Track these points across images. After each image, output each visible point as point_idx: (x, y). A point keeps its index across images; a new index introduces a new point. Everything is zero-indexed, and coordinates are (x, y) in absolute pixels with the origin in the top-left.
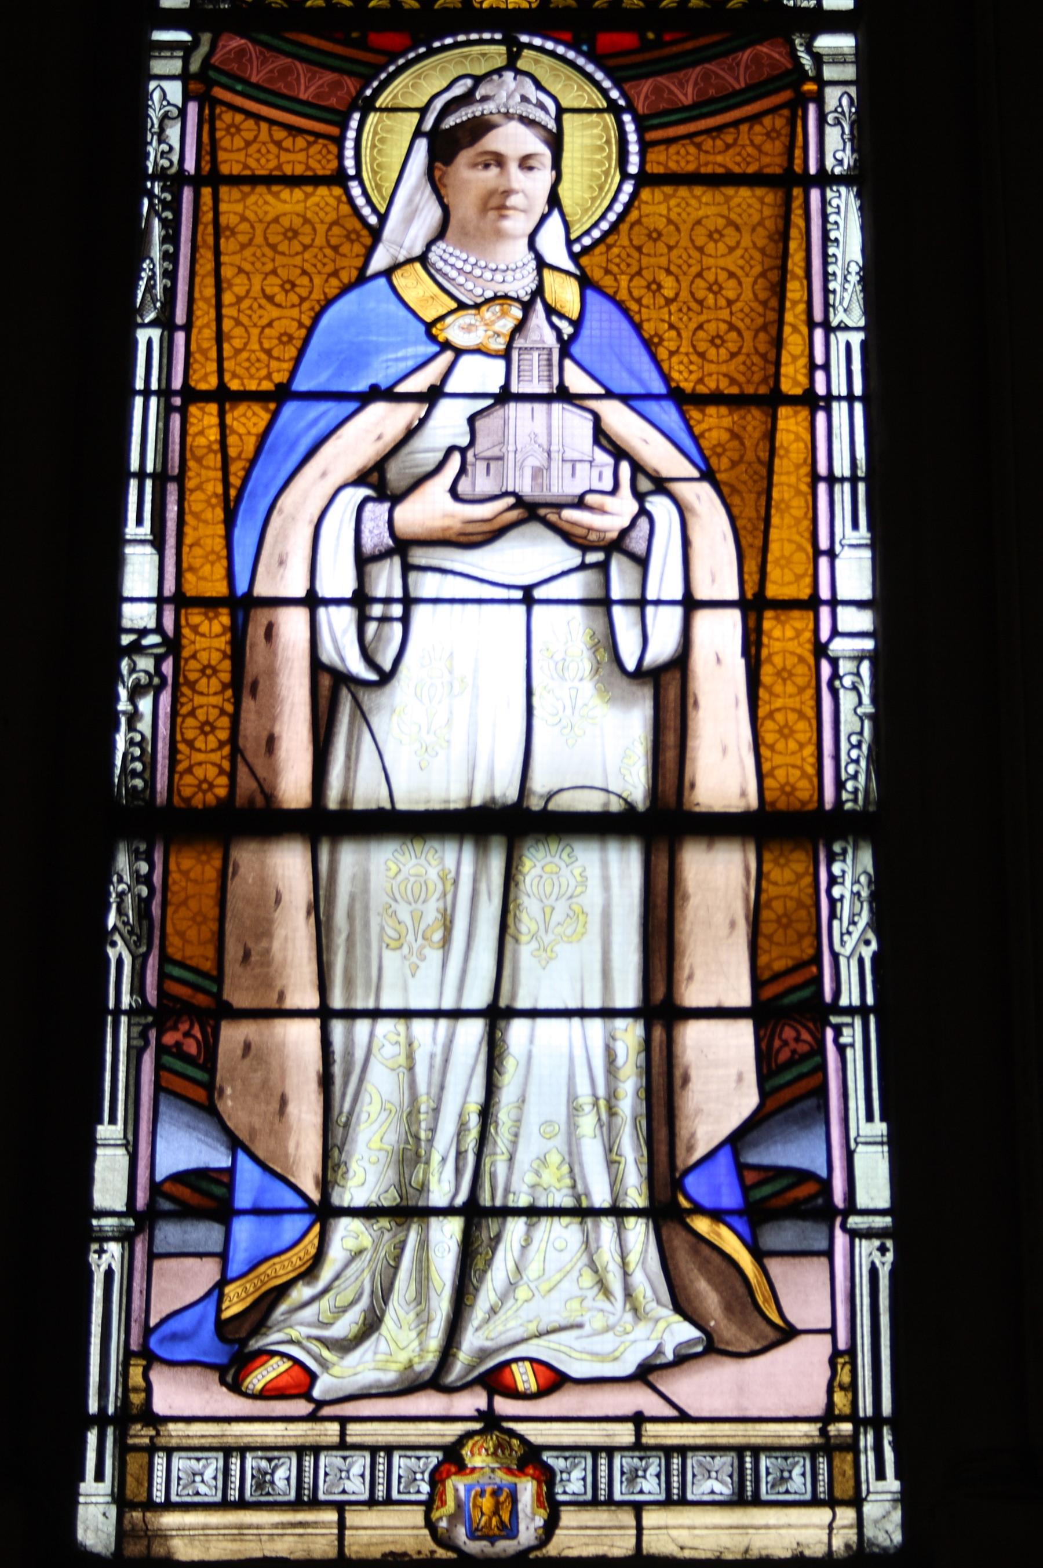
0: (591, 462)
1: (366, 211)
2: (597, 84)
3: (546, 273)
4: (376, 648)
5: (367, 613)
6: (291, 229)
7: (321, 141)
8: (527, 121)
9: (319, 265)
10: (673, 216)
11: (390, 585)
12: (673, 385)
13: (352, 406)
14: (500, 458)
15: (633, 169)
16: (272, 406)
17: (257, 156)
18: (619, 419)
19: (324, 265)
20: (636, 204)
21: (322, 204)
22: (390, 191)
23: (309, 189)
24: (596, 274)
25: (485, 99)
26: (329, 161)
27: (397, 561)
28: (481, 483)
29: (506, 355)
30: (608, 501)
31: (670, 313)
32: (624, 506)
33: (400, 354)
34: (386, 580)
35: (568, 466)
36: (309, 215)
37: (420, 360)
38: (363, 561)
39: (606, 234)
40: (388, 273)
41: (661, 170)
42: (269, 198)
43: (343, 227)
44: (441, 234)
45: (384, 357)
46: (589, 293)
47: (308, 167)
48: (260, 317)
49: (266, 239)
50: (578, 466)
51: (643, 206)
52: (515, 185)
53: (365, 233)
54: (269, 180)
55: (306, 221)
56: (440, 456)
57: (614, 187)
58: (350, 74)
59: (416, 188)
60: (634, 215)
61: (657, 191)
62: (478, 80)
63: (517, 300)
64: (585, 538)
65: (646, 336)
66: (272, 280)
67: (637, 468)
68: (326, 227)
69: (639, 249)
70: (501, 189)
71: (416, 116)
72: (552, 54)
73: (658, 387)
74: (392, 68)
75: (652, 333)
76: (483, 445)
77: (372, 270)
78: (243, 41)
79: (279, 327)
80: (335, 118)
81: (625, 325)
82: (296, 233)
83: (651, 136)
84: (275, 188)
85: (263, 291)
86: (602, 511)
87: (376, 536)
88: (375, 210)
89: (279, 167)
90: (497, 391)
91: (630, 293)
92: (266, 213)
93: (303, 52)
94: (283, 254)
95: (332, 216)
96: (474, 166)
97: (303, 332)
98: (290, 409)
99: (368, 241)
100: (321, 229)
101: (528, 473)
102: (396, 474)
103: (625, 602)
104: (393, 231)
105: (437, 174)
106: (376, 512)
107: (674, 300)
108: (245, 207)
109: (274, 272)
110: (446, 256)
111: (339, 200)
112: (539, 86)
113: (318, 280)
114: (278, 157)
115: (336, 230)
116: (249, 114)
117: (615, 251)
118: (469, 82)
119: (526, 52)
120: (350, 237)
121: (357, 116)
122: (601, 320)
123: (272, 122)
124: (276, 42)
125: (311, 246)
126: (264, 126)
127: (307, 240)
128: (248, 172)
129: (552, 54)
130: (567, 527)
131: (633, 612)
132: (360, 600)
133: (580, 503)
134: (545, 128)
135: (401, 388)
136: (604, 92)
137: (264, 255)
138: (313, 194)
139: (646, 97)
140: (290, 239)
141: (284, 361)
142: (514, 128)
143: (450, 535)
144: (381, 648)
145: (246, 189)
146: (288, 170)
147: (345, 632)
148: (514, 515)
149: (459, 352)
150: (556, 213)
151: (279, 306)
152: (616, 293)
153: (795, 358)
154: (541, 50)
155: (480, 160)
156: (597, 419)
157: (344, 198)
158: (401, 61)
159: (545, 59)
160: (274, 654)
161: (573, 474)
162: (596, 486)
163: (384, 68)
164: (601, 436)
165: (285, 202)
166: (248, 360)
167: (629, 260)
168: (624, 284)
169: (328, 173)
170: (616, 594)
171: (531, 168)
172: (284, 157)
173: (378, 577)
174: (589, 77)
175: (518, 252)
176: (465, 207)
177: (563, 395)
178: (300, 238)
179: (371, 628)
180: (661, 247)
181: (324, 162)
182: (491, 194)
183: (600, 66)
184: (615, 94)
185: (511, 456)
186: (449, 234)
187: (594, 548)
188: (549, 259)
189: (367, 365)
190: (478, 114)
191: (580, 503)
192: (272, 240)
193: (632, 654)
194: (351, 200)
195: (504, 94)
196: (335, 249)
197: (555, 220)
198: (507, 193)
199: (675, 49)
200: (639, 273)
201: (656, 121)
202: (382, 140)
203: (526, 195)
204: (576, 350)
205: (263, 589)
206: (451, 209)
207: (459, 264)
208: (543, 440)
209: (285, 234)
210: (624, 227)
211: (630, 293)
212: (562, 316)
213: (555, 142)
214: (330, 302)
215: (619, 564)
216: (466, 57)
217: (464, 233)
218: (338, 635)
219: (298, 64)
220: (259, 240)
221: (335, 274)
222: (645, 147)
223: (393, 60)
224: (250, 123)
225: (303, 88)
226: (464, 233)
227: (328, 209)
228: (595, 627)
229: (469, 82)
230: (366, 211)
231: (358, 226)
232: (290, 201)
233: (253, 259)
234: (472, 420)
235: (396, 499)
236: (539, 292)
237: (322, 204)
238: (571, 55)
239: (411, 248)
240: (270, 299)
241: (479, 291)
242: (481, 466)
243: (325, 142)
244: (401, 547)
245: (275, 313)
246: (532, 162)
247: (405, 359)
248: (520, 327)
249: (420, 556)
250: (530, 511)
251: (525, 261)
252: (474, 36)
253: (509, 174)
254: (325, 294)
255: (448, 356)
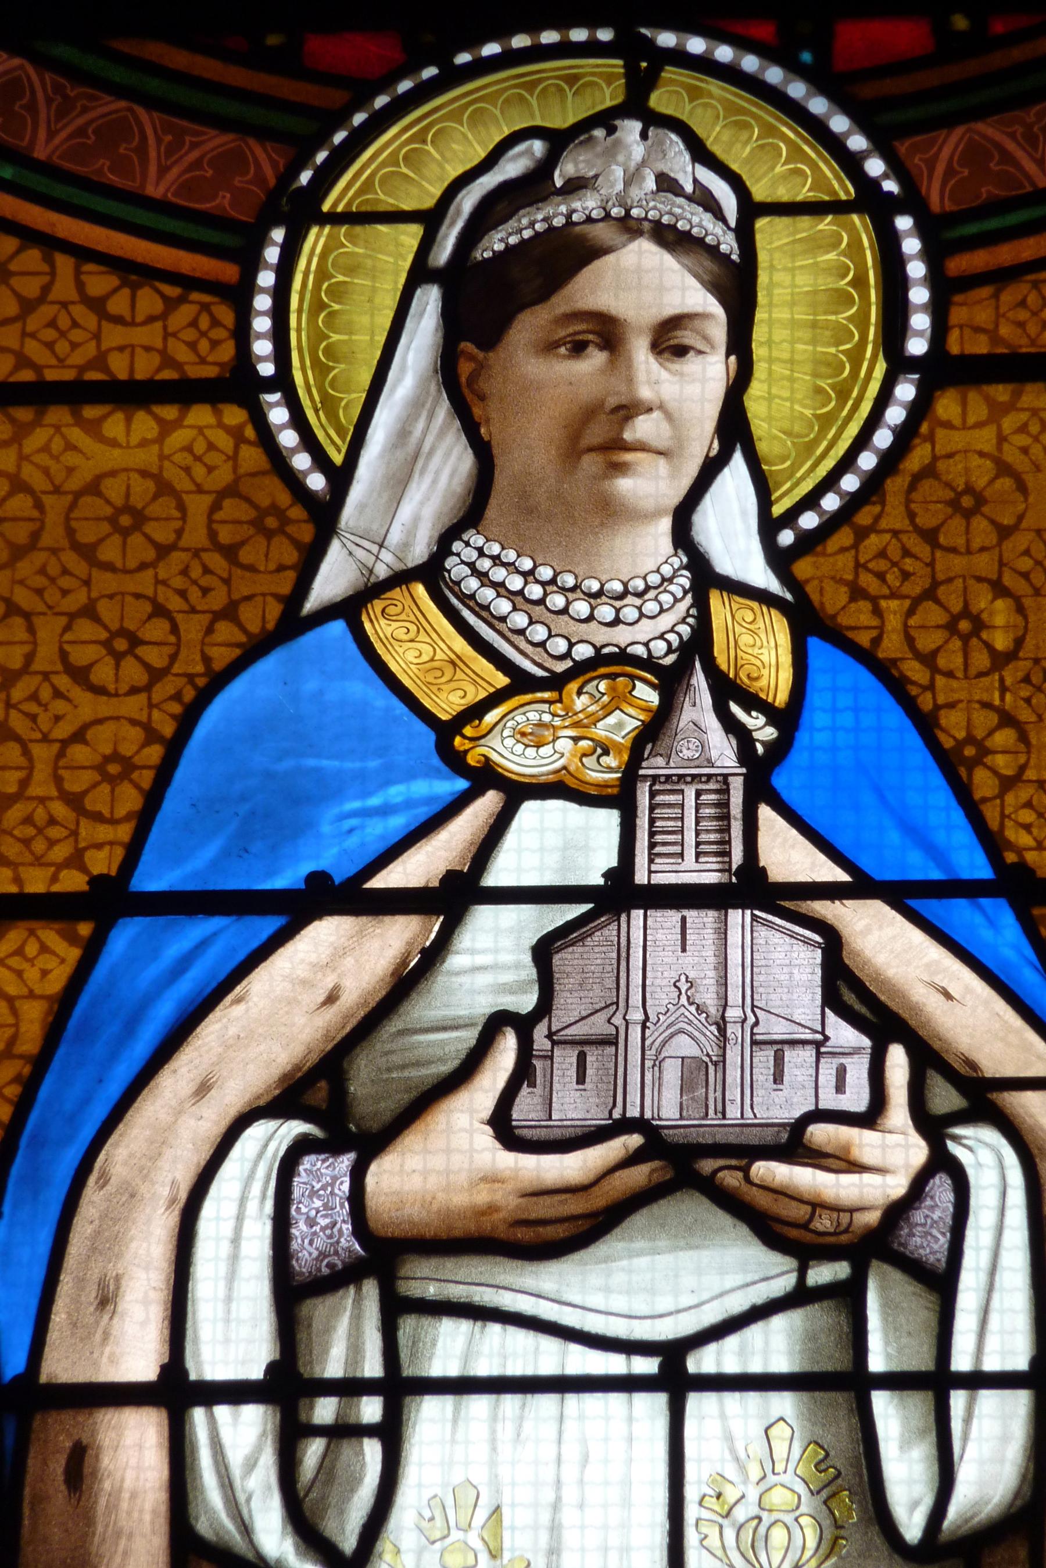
0: (818, 1045)
1: (302, 461)
2: (834, 145)
3: (716, 601)
4: (324, 1497)
5: (303, 1417)
6: (127, 508)
7: (195, 296)
8: (672, 238)
9: (194, 594)
10: (1011, 455)
11: (355, 1350)
12: (1011, 857)
13: (269, 925)
14: (610, 1041)
15: (917, 347)
16: (85, 929)
17: (50, 334)
18: (886, 942)
19: (205, 591)
20: (924, 428)
21: (200, 447)
22: (356, 412)
23: (169, 412)
24: (832, 599)
25: (576, 186)
26: (215, 344)
27: (371, 1289)
28: (573, 1105)
29: (621, 798)
30: (865, 1143)
31: (1003, 689)
32: (896, 1151)
33: (374, 801)
34: (348, 1340)
35: (765, 1057)
36: (171, 473)
37: (423, 813)
38: (293, 1292)
39: (853, 503)
40: (350, 609)
41: (981, 346)
42: (76, 434)
43: (248, 500)
44: (472, 513)
45: (335, 811)
46: (814, 643)
47: (168, 361)
48: (57, 718)
49: (71, 532)
50: (791, 1056)
51: (940, 433)
52: (645, 393)
53: (297, 512)
54: (76, 394)
55: (164, 488)
56: (469, 1037)
57: (874, 388)
58: (264, 134)
59: (416, 406)
60: (918, 457)
61: (973, 396)
62: (559, 141)
63: (648, 664)
64: (805, 1226)
65: (948, 743)
66: (85, 629)
67: (927, 1058)
68: (207, 500)
69: (930, 536)
70: (612, 402)
71: (411, 235)
72: (730, 74)
73: (975, 865)
74: (359, 118)
75: (961, 735)
76: (569, 1007)
77: (312, 603)
78: (16, 61)
79: (103, 739)
80: (228, 241)
81: (895, 717)
82: (140, 518)
83: (958, 264)
84: (90, 412)
85: (64, 655)
86: (847, 1163)
87: (323, 1228)
88: (321, 461)
89: (100, 361)
90: (596, 879)
91: (910, 641)
92: (70, 470)
93: (154, 85)
94: (109, 567)
95: (224, 476)
96: (549, 347)
97: (154, 753)
98: (126, 936)
99: (306, 533)
100: (198, 506)
101: (672, 1073)
102: (368, 1082)
103: (896, 1381)
104: (362, 507)
105: (465, 368)
106: (326, 1176)
107: (1011, 656)
108: (22, 458)
109: (89, 612)
110: (485, 564)
111: (237, 435)
112: (701, 153)
113: (192, 628)
114: (97, 336)
115: (231, 508)
116: (30, 236)
117: (874, 542)
118: (538, 147)
119: (670, 73)
120: (265, 524)
121: (278, 235)
122: (834, 710)
123: (83, 254)
124: (91, 63)
125: (173, 547)
126: (64, 263)
127: (163, 534)
128: (26, 376)
129: (730, 74)
130: (763, 1200)
131: (920, 1403)
132: (285, 1387)
133: (792, 1144)
134: (713, 251)
135: (380, 882)
136: (851, 164)
137: (65, 572)
138: (178, 424)
139: (949, 172)
140: (125, 533)
141: (113, 821)
142: (644, 255)
143: (495, 1225)
144: (333, 1500)
145: (24, 414)
146: (119, 367)
147: (251, 1464)
148: (639, 1175)
149: (518, 792)
150: (738, 459)
151: (100, 691)
152: (877, 641)
153: (949, 828)
154: (705, 65)
155: (562, 333)
156: (832, 943)
157: (250, 432)
158: (381, 101)
159: (715, 87)
160: (88, 1519)
161: (778, 1077)
162: (829, 1101)
163: (341, 118)
164: (845, 986)
165: (114, 443)
166: (28, 820)
167: (909, 564)
168: (894, 622)
169: (210, 372)
170: (877, 1363)
171: (681, 351)
172: (114, 336)
173: (328, 1329)
174: (817, 129)
175: (651, 549)
176: (529, 446)
177: (750, 889)
178: (149, 528)
179: (314, 1450)
180: (982, 530)
181: (204, 345)
182: (590, 413)
183: (843, 103)
184: (875, 167)
185: (635, 1033)
186: (491, 512)
187: (830, 1253)
188: (725, 564)
189: (307, 827)
190: (558, 222)
191: (792, 1144)
192: (87, 534)
193: (914, 1505)
194: (266, 436)
195: (618, 172)
196: (230, 552)
197: (735, 480)
198: (629, 410)
199: (1018, 54)
200: (930, 594)
201: (971, 229)
202: (338, 292)
203: (669, 416)
204: (781, 780)
205: (61, 1366)
206: (499, 461)
207: (516, 583)
208: (709, 997)
209: (113, 520)
210: (895, 485)
211: (910, 641)
212: (752, 702)
213: (737, 285)
214: (219, 680)
215: (883, 1289)
216: (531, 86)
217: (527, 508)
218: (236, 1472)
219: (141, 112)
220: (53, 535)
221: (229, 612)
222: (944, 291)
223: (361, 101)
224: (33, 257)
225: (153, 169)
226: (527, 508)
227: (212, 458)
228: (827, 1440)
229: (538, 147)
230: (302, 461)
231: (284, 497)
232: (127, 441)
233: (40, 581)
234: (544, 952)
235: (369, 1144)
236: (698, 644)
237: (200, 447)
238: (774, 75)
239: (406, 545)
240: (80, 675)
241: (560, 646)
242: (566, 1060)
243: (206, 298)
244: (383, 1256)
245: (87, 707)
246: (687, 337)
247: (385, 811)
248: (655, 729)
249: (426, 1280)
250: (685, 1169)
251: (667, 571)
252: (549, 37)
253: (629, 366)
254: (206, 660)
255: (490, 801)
